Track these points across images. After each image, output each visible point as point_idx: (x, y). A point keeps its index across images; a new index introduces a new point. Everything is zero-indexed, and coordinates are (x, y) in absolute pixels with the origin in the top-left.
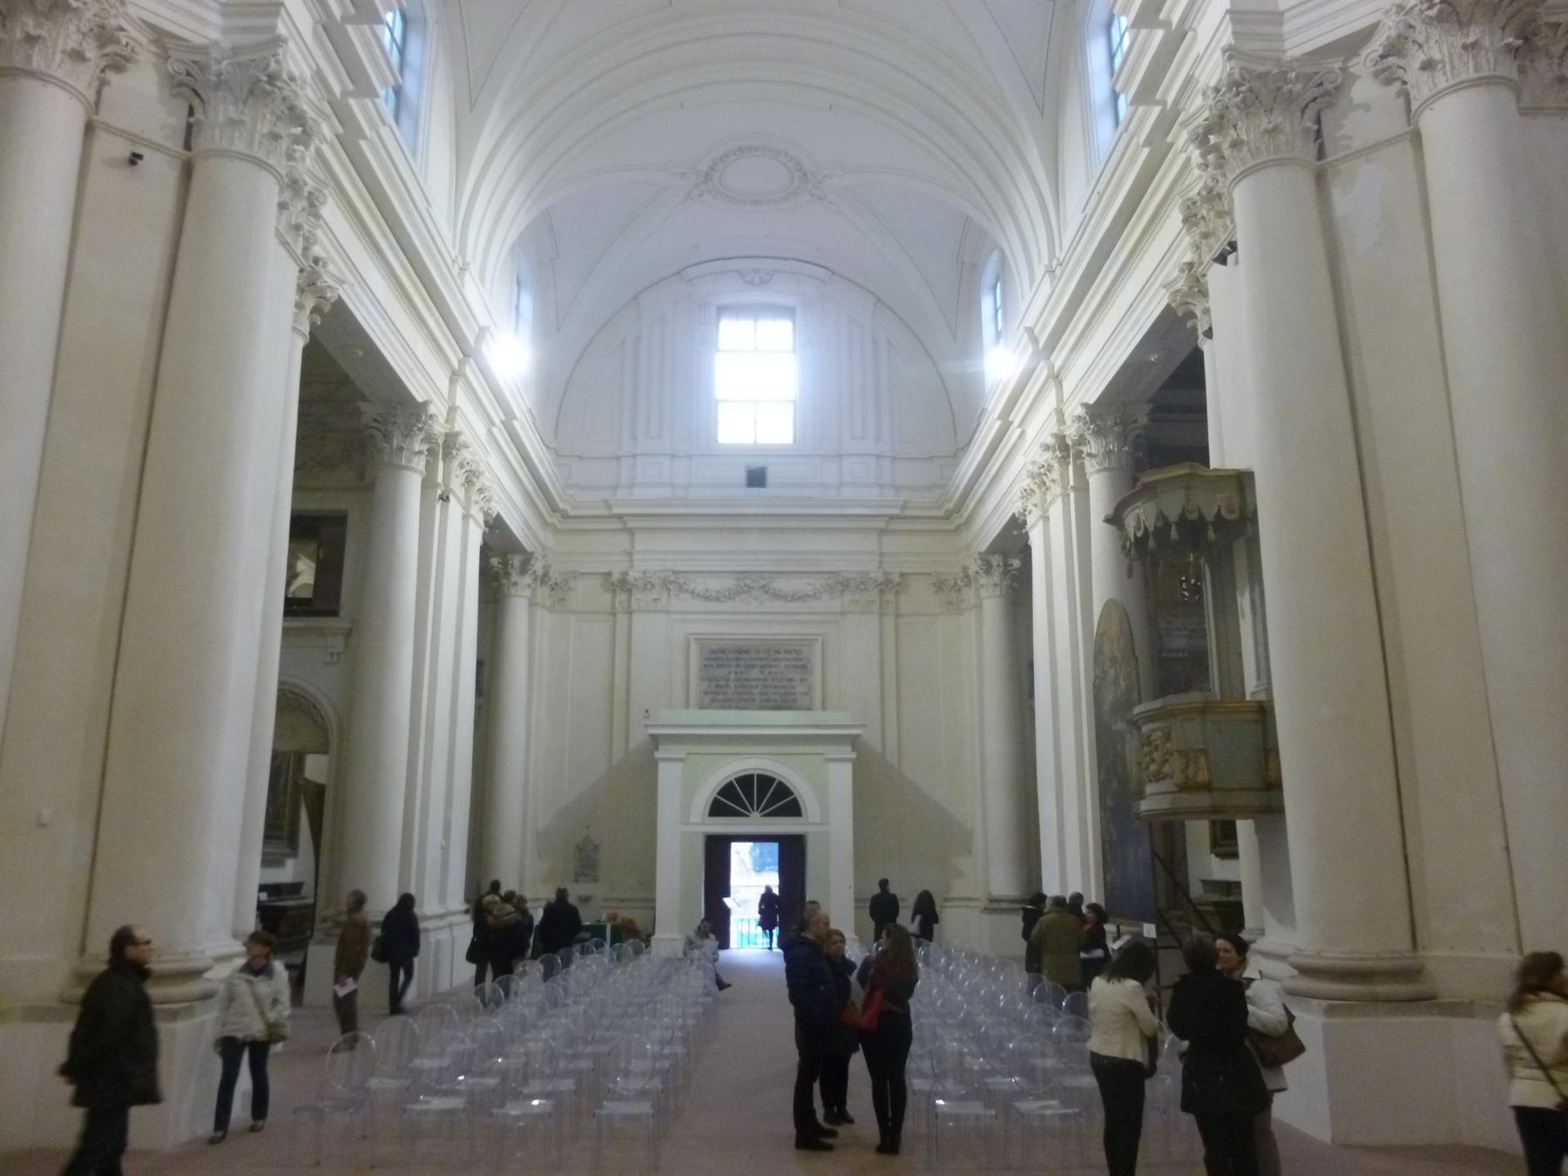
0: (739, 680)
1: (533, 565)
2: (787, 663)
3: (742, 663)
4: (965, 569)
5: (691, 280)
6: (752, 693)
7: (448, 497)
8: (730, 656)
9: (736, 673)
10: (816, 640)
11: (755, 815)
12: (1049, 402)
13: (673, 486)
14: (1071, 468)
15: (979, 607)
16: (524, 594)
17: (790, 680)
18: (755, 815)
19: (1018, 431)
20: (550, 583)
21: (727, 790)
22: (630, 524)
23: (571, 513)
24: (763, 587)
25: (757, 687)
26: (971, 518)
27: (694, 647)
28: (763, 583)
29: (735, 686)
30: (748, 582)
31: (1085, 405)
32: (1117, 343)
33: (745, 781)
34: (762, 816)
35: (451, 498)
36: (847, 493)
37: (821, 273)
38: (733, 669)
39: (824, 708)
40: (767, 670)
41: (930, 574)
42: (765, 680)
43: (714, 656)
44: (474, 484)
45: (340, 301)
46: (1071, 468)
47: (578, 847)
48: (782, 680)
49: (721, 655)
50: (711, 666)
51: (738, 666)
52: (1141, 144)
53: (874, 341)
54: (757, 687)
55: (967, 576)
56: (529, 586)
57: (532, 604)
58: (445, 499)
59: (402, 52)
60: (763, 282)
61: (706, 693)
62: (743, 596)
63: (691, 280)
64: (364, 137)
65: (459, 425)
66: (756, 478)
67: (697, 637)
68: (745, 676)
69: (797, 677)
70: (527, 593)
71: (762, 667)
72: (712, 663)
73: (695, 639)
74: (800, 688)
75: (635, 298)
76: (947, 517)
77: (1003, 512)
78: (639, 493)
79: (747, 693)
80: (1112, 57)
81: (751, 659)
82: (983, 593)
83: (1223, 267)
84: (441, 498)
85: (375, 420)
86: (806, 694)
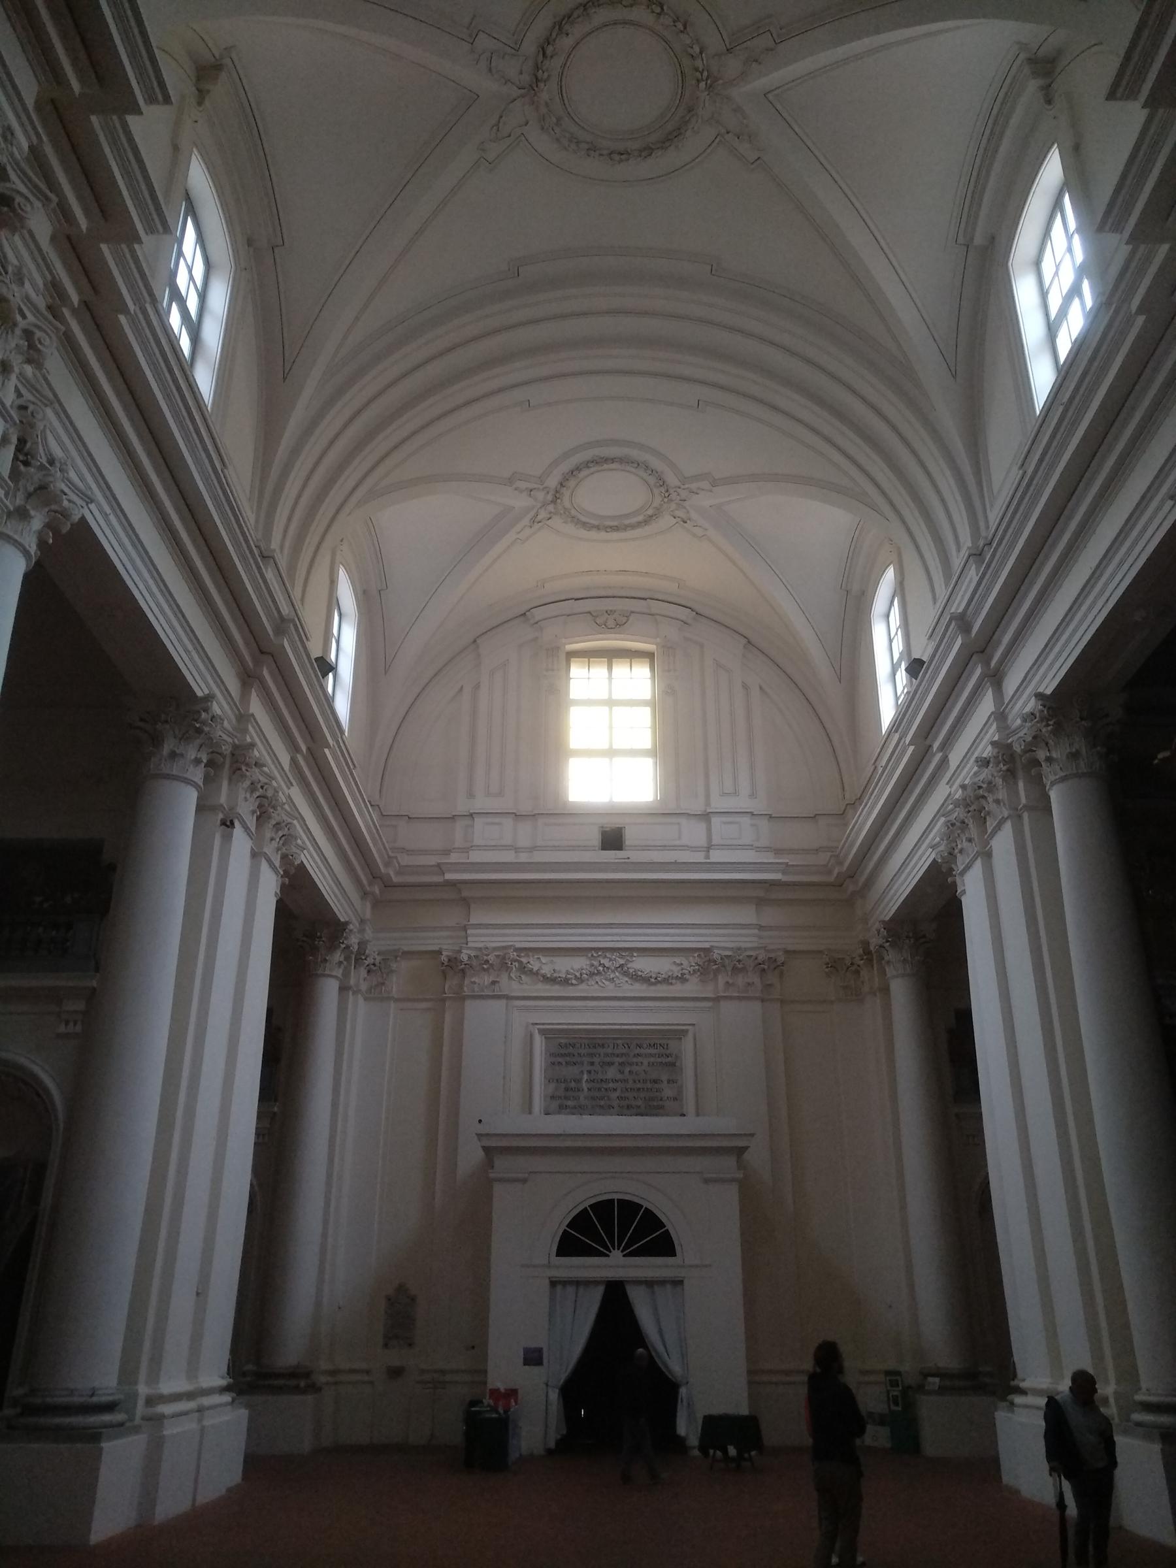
0: (593, 1081)
1: (346, 938)
2: (652, 1060)
3: (596, 1060)
4: (865, 944)
5: (537, 623)
6: (609, 1099)
7: (232, 823)
8: (582, 1051)
9: (589, 1072)
10: (687, 1031)
11: (616, 1255)
12: (987, 705)
13: (517, 850)
14: (1021, 784)
15: (885, 990)
16: (334, 973)
17: (655, 1081)
18: (616, 1255)
19: (938, 756)
20: (366, 963)
21: (580, 1221)
22: (465, 894)
23: (396, 879)
24: (622, 966)
25: (615, 1090)
26: (869, 883)
27: (539, 1042)
28: (622, 962)
29: (589, 1089)
30: (606, 962)
31: (1039, 696)
32: (1048, 661)
33: (603, 1208)
34: (624, 1256)
35: (236, 823)
36: (716, 856)
37: (683, 613)
38: (586, 1068)
39: (698, 1115)
40: (627, 1069)
41: (820, 952)
42: (626, 1081)
43: (563, 1051)
44: (270, 817)
45: (83, 519)
46: (1021, 784)
47: (389, 1299)
48: (645, 1081)
49: (571, 1050)
50: (560, 1063)
51: (592, 1064)
52: (1133, 312)
53: (745, 687)
54: (615, 1090)
55: (867, 952)
56: (340, 963)
57: (343, 989)
58: (228, 824)
59: (203, 296)
60: (619, 625)
61: (552, 1097)
62: (597, 978)
63: (537, 623)
64: (125, 310)
65: (252, 735)
66: (613, 839)
67: (541, 1027)
68: (600, 1076)
69: (664, 1078)
70: (339, 972)
71: (621, 1064)
72: (560, 1060)
73: (541, 1032)
74: (668, 1092)
75: (475, 641)
76: (839, 885)
77: (897, 891)
78: (476, 857)
79: (602, 1098)
80: (1044, 294)
81: (607, 1055)
82: (890, 971)
83: (522, 1364)
84: (223, 823)
85: (142, 720)
86: (675, 1099)
